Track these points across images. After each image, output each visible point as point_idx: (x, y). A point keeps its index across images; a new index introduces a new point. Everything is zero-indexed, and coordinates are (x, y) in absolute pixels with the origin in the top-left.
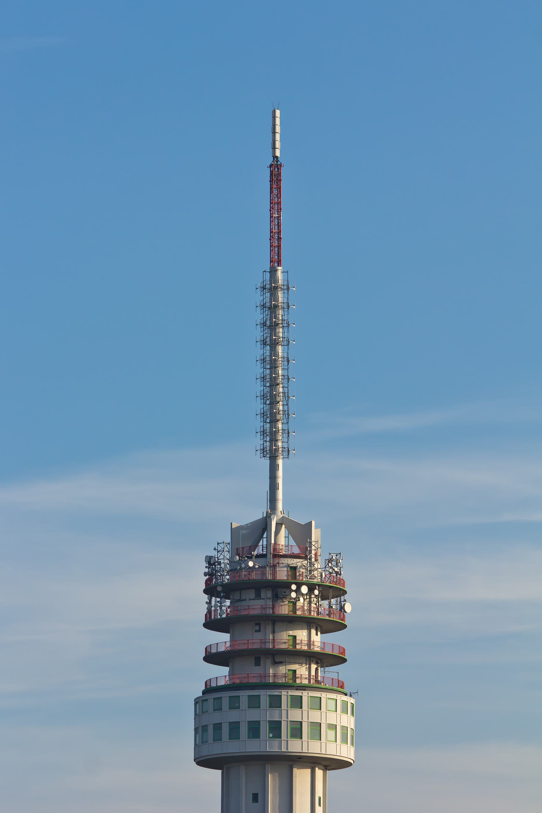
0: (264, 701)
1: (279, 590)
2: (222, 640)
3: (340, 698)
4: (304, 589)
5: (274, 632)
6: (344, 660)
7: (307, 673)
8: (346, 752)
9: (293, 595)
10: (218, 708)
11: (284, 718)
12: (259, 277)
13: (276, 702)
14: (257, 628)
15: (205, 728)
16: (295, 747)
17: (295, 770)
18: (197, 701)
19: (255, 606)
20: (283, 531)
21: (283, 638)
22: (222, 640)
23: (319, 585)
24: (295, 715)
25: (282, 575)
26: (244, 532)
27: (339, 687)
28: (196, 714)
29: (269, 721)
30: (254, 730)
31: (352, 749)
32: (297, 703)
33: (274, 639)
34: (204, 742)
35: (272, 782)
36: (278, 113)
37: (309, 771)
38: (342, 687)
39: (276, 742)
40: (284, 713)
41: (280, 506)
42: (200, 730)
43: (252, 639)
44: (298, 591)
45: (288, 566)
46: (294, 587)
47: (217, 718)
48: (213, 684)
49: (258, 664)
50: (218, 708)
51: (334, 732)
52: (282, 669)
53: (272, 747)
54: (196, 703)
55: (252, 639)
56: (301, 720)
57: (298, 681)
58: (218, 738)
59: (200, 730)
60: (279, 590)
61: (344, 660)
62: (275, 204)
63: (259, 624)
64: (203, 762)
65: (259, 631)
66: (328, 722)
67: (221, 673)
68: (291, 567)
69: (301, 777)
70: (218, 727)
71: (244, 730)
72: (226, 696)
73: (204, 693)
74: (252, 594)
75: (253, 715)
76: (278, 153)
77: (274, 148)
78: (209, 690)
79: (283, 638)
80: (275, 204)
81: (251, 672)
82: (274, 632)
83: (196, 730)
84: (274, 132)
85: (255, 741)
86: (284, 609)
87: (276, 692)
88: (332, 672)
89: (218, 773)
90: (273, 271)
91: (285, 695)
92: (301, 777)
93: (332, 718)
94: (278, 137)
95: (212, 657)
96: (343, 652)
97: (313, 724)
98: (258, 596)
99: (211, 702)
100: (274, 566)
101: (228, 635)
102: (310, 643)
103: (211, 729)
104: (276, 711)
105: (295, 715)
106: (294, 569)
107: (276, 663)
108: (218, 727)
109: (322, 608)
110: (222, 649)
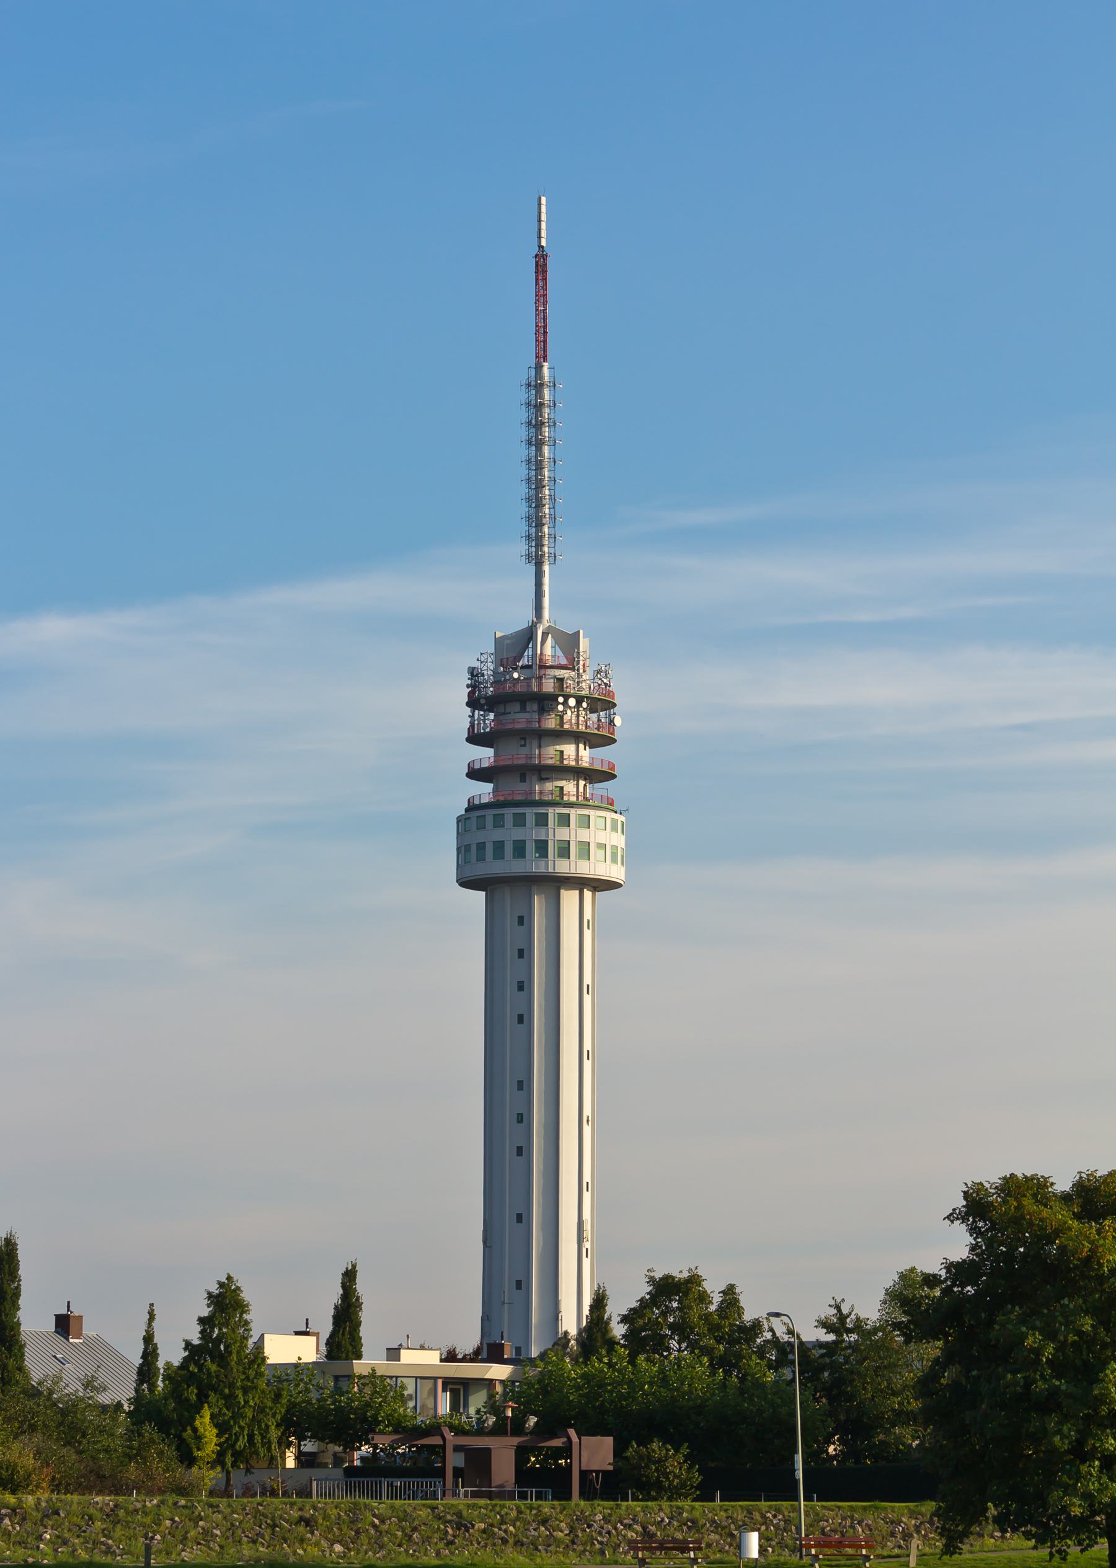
0: (530, 819)
1: (546, 702)
2: (485, 755)
3: (610, 816)
4: (572, 702)
6: (614, 777)
8: (616, 873)
9: (561, 708)
10: (482, 827)
11: (551, 837)
12: (525, 374)
13: (542, 820)
14: (523, 742)
15: (468, 848)
16: (562, 867)
17: (562, 891)
18: (459, 820)
19: (520, 719)
21: (550, 753)
22: (485, 755)
24: (562, 834)
25: (549, 686)
27: (608, 804)
30: (520, 850)
31: (623, 870)
32: (565, 821)
33: (540, 754)
35: (539, 903)
36: (544, 200)
37: (577, 892)
38: (612, 804)
39: (542, 863)
40: (551, 831)
42: (463, 850)
43: (517, 754)
44: (565, 703)
45: (555, 677)
46: (561, 699)
47: (481, 836)
48: (477, 802)
50: (482, 827)
52: (549, 786)
53: (538, 867)
54: (458, 822)
55: (517, 754)
57: (566, 798)
58: (481, 858)
59: (463, 849)
60: (546, 702)
61: (614, 777)
62: (541, 297)
63: (524, 739)
64: (467, 883)
65: (525, 745)
67: (484, 791)
69: (569, 898)
70: (481, 846)
71: (509, 849)
72: (489, 814)
73: (467, 810)
76: (544, 243)
77: (540, 237)
78: (472, 807)
79: (550, 753)
80: (541, 297)
81: (516, 789)
82: (540, 747)
83: (458, 849)
84: (540, 221)
85: (520, 861)
87: (542, 810)
88: (602, 788)
89: (481, 895)
90: (539, 368)
91: (552, 813)
92: (569, 898)
95: (475, 774)
96: (613, 768)
98: (523, 709)
100: (540, 678)
102: (577, 759)
103: (474, 848)
104: (543, 830)
105: (562, 834)
106: (561, 680)
107: (543, 779)
108: (481, 846)
110: (485, 764)
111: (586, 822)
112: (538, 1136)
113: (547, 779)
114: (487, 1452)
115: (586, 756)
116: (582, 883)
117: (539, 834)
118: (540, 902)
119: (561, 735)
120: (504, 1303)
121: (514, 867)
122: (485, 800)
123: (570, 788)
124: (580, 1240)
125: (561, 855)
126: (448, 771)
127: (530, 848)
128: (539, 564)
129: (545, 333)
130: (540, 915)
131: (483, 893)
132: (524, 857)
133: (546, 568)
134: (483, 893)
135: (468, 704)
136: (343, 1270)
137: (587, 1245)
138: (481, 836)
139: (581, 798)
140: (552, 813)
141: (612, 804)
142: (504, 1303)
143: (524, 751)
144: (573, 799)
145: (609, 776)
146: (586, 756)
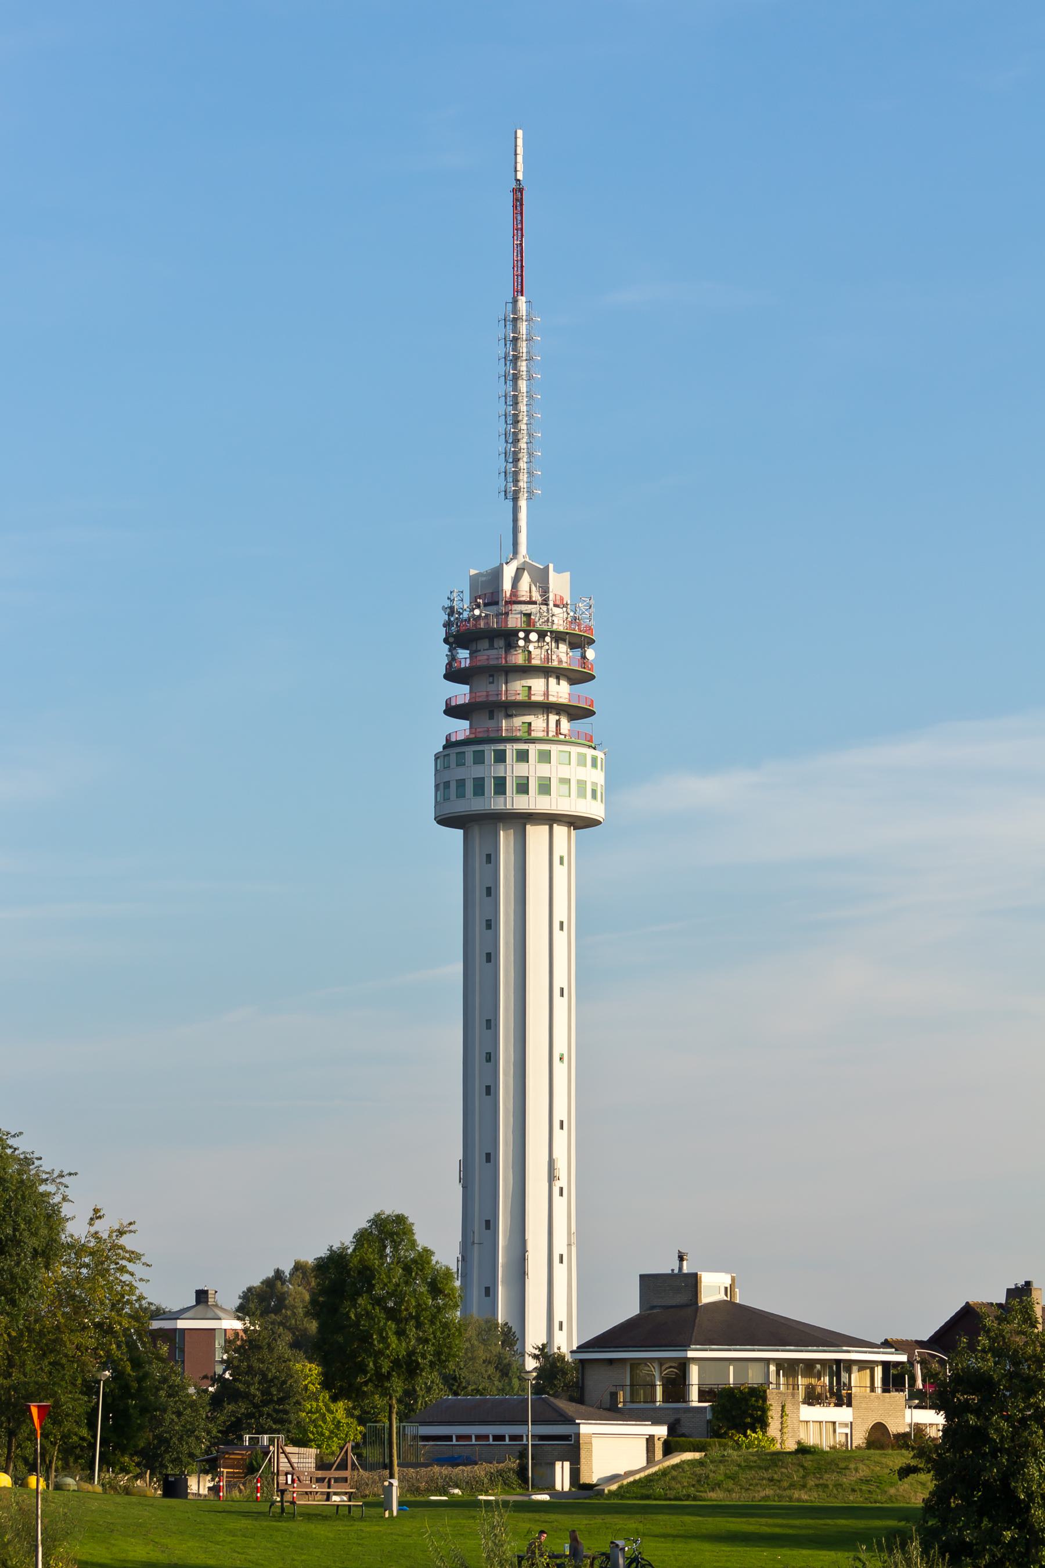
0: (490, 757)
1: (509, 638)
2: (461, 693)
3: (590, 752)
4: (534, 636)
5: (506, 683)
6: (592, 713)
7: (545, 725)
8: (594, 809)
9: (521, 643)
10: (461, 763)
11: (509, 773)
12: (502, 309)
13: (501, 757)
14: (491, 679)
15: (447, 785)
16: (521, 803)
17: (528, 827)
18: (437, 757)
19: (489, 655)
20: (526, 579)
21: (516, 689)
22: (461, 693)
23: (551, 632)
24: (521, 769)
25: (514, 621)
26: (484, 579)
27: (590, 742)
28: (436, 770)
29: (494, 778)
30: (479, 787)
31: (602, 807)
32: (545, 757)
33: (507, 690)
34: (446, 799)
35: (505, 839)
36: (520, 133)
37: (547, 827)
38: (591, 741)
39: (501, 799)
40: (509, 768)
41: (523, 549)
42: (442, 787)
43: (485, 691)
44: (527, 639)
45: (521, 613)
46: (521, 635)
47: (459, 773)
48: (453, 739)
49: (491, 717)
50: (461, 763)
51: (567, 786)
52: (518, 721)
53: (497, 804)
54: (436, 759)
55: (485, 691)
56: (503, 775)
57: (534, 734)
58: (461, 795)
59: (442, 786)
60: (509, 638)
61: (592, 713)
62: (519, 230)
63: (492, 676)
64: (446, 821)
65: (493, 683)
66: (538, 775)
67: (461, 728)
68: (525, 614)
69: (536, 834)
70: (461, 783)
71: (490, 786)
72: (469, 750)
73: (445, 747)
74: (485, 644)
75: (477, 771)
76: (520, 176)
77: (516, 171)
78: (449, 744)
79: (516, 689)
80: (519, 230)
81: (486, 724)
82: (506, 683)
83: (437, 786)
84: (516, 154)
85: (479, 799)
86: (519, 659)
87: (501, 747)
88: (583, 725)
89: (460, 833)
90: (515, 301)
91: (511, 749)
92: (536, 834)
93: (564, 772)
94: (520, 159)
95: (453, 711)
96: (592, 705)
97: (579, 782)
98: (492, 647)
99: (453, 758)
100: (507, 614)
101: (468, 687)
102: (547, 694)
103: (453, 786)
104: (501, 766)
105: (521, 769)
106: (528, 615)
107: (509, 716)
108: (461, 783)
109: (563, 655)
110: (460, 701)
111: (545, 757)
112: (506, 1074)
113: (516, 716)
114: (903, 1391)
115: (561, 691)
116: (550, 819)
117: (499, 771)
118: (506, 838)
119: (528, 670)
120: (473, 1243)
121: (475, 805)
122: (461, 737)
123: (538, 723)
124: (552, 1177)
125: (475, 794)
126: (425, 709)
127: (490, 786)
128: (515, 500)
129: (522, 266)
130: (507, 852)
131: (462, 831)
132: (483, 794)
133: (523, 503)
134: (462, 831)
135: (446, 641)
136: (378, 1212)
137: (562, 1182)
138: (459, 773)
139: (551, 734)
140: (511, 749)
141: (591, 741)
142: (473, 1243)
143: (491, 688)
144: (540, 734)
145: (589, 713)
146: (561, 691)
